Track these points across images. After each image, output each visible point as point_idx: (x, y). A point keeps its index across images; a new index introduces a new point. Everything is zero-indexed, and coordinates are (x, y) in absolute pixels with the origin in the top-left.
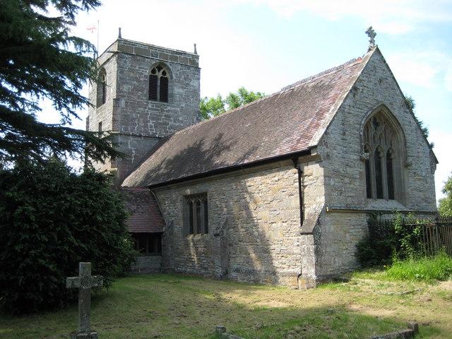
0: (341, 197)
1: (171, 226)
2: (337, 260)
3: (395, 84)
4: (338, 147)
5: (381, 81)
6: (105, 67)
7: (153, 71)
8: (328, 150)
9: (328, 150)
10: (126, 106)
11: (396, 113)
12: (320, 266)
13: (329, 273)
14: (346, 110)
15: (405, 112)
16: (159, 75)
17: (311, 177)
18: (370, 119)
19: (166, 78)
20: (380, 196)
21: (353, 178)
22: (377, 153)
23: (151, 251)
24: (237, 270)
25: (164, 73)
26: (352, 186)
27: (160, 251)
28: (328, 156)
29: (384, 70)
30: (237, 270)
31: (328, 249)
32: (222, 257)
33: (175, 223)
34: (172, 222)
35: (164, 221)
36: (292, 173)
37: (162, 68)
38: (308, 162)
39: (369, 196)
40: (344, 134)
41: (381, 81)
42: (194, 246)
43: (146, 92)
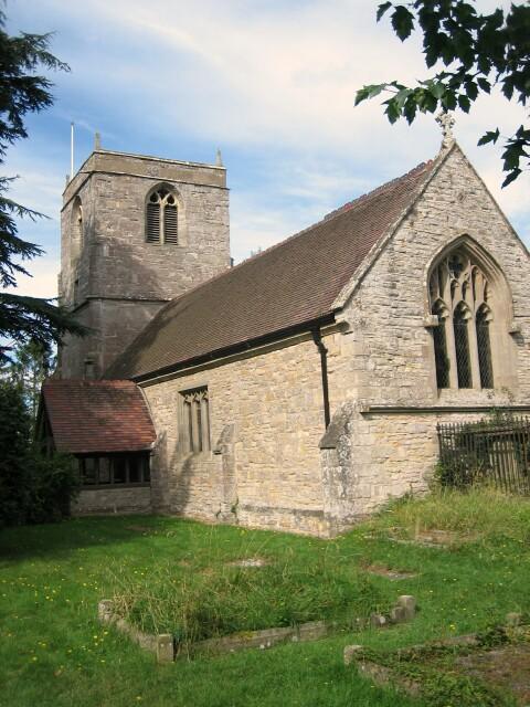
0: (388, 389)
1: (162, 442)
2: (381, 490)
3: (489, 200)
4: (383, 308)
5: (461, 197)
6: (79, 195)
7: (154, 198)
8: (364, 314)
9: (364, 314)
10: (111, 254)
11: (491, 248)
12: (350, 500)
13: (365, 511)
14: (396, 248)
15: (510, 244)
16: (163, 202)
17: (338, 358)
18: (446, 259)
19: (175, 208)
20: (464, 382)
21: (411, 357)
22: (459, 314)
23: (134, 479)
24: (248, 508)
25: (171, 200)
26: (407, 369)
27: (148, 479)
28: (363, 323)
29: (467, 179)
30: (248, 508)
31: (364, 473)
32: (225, 488)
33: (168, 434)
34: (165, 433)
35: (154, 432)
36: (306, 351)
37: (167, 193)
38: (330, 331)
39: (442, 382)
40: (394, 287)
41: (461, 197)
42: (451, 443)
43: (141, 231)
